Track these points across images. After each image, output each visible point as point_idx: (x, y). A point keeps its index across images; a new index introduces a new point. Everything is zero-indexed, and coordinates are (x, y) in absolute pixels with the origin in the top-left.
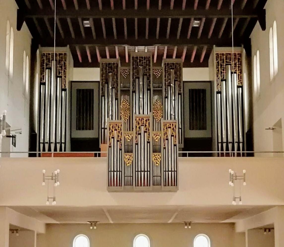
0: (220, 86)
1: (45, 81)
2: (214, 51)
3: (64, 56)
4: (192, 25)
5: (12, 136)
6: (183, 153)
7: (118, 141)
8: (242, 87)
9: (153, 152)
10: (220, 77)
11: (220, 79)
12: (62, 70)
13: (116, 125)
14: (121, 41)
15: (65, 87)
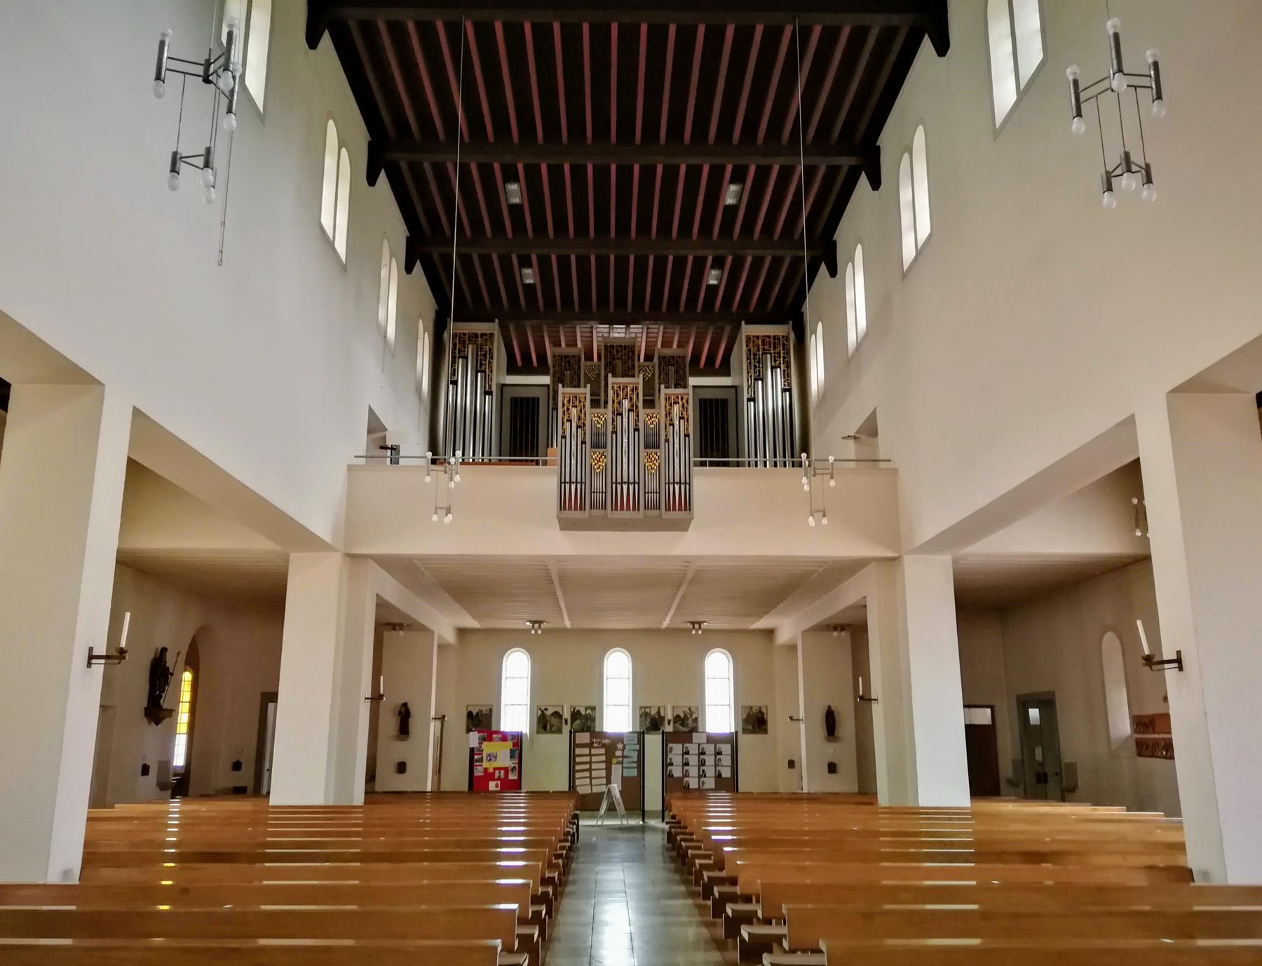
0: (753, 389)
1: (456, 379)
3: (490, 337)
5: (390, 446)
6: (701, 462)
7: (578, 427)
8: (790, 390)
9: (646, 447)
10: (753, 375)
11: (753, 378)
12: (486, 361)
14: (586, 314)
15: (491, 388)
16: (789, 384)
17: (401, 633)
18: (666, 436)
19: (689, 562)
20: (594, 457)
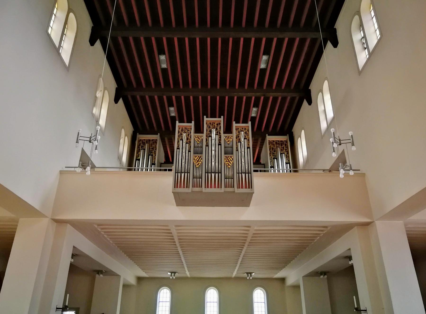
2: (267, 139)
4: (251, 115)
9: (225, 154)
13: (186, 128)
15: (155, 162)
16: (289, 161)
17: (101, 276)
18: (237, 148)
19: (249, 227)
20: (195, 159)
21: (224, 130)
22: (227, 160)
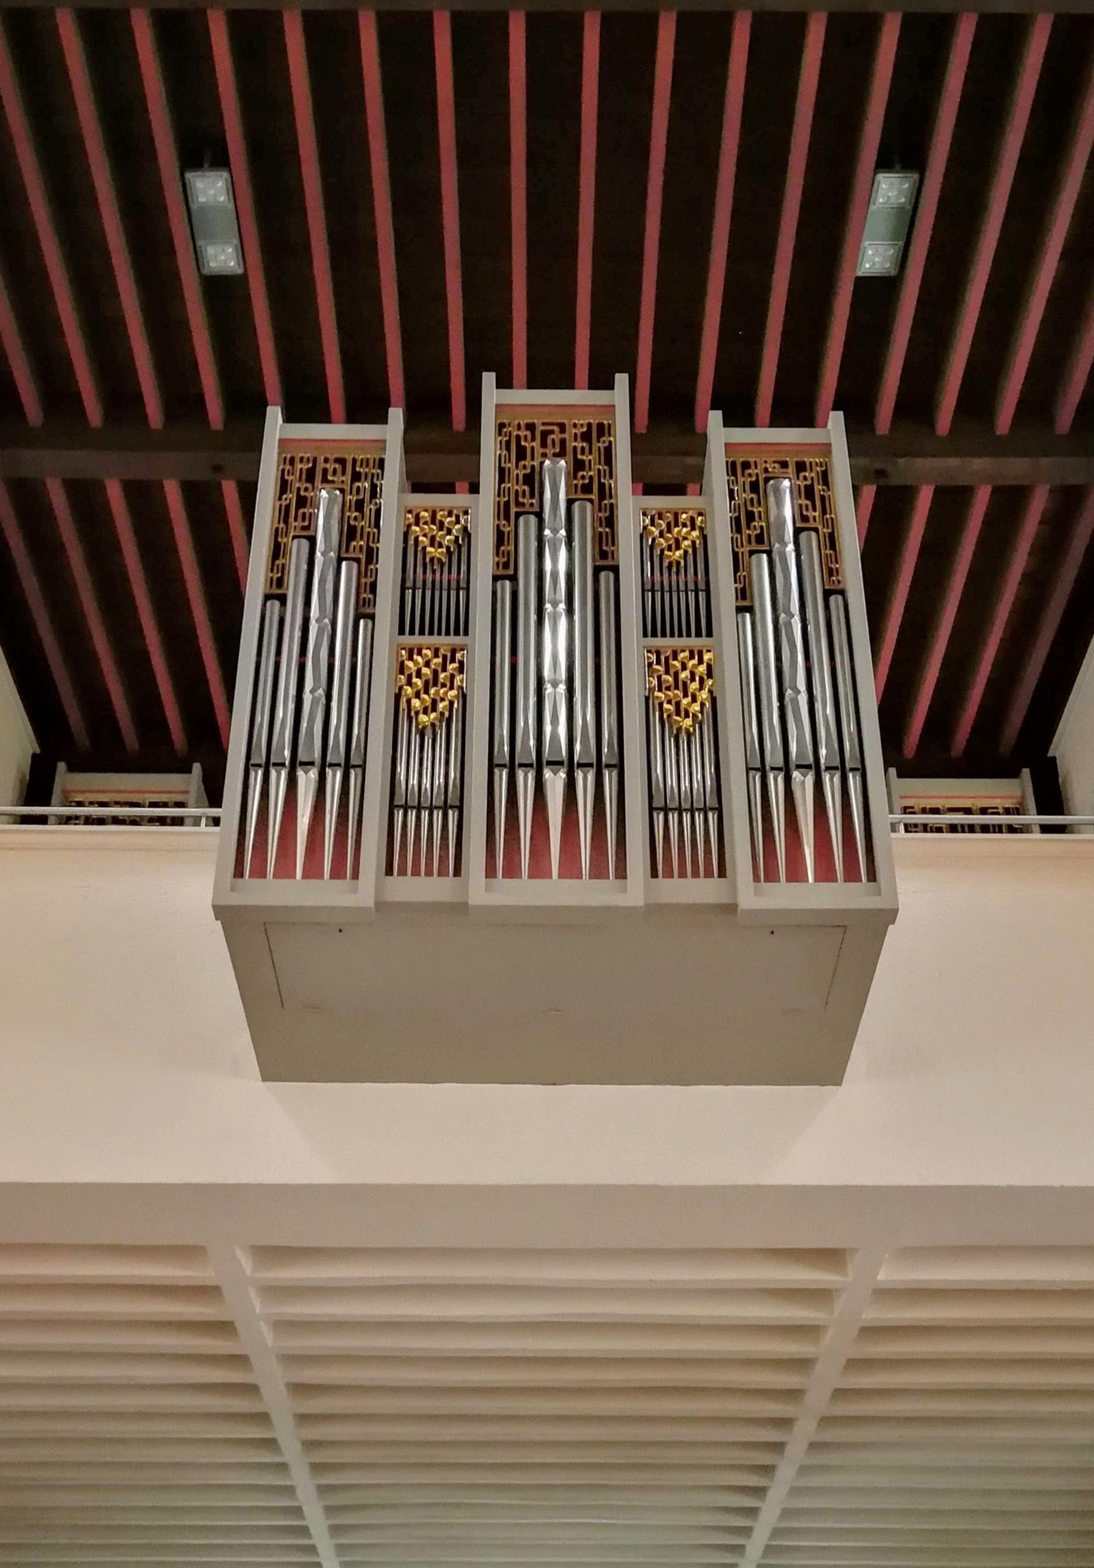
9: (651, 629)
21: (637, 421)
22: (664, 677)
